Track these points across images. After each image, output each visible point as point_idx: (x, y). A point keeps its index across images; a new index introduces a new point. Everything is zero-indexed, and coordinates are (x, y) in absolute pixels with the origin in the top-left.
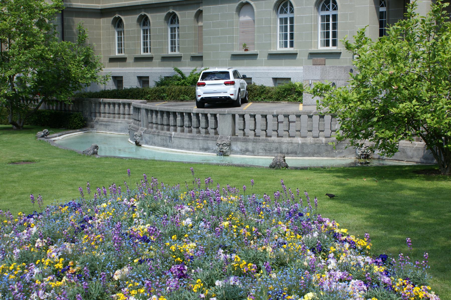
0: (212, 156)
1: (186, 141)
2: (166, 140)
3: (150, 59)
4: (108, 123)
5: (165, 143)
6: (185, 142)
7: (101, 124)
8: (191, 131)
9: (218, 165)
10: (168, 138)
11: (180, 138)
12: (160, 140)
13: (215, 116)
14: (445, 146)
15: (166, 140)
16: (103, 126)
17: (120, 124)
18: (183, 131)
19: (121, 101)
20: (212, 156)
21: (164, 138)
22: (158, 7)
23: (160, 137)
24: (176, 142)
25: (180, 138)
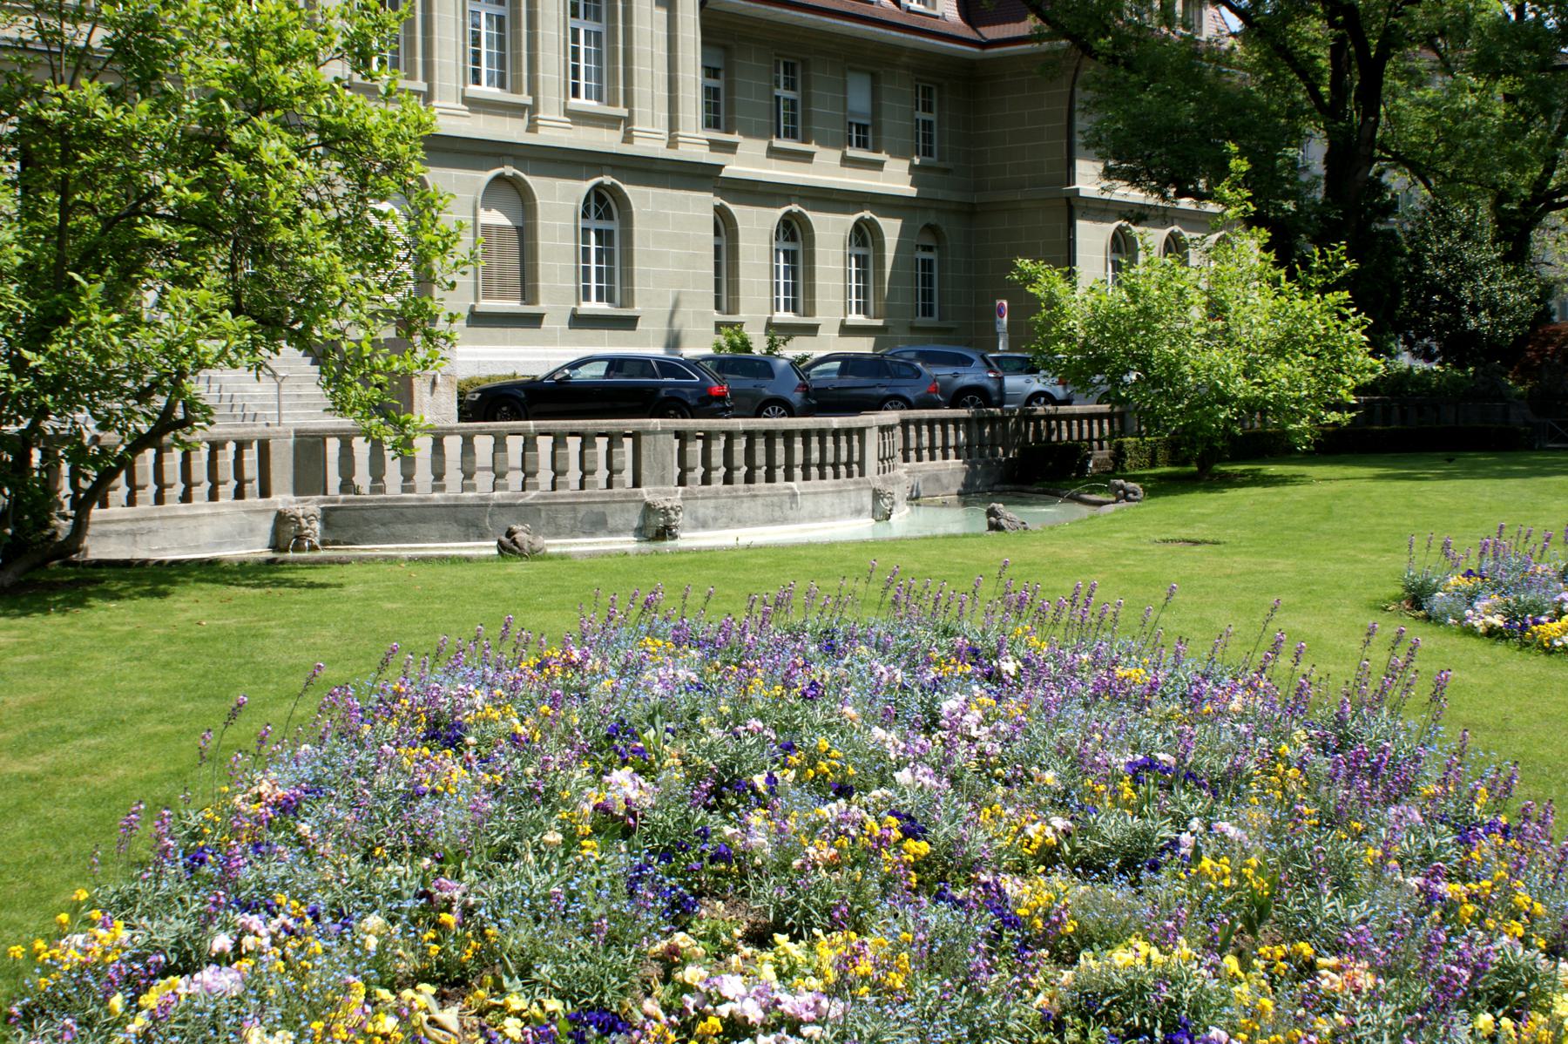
0: (861, 527)
1: (828, 499)
2: (781, 507)
3: (535, 320)
4: (143, 524)
5: (777, 514)
6: (826, 502)
7: (104, 535)
8: (837, 476)
9: (965, 536)
10: (786, 499)
11: (816, 493)
12: (760, 509)
13: (636, 436)
14: (60, 453)
15: (781, 507)
16: (113, 540)
17: (208, 520)
18: (822, 476)
19: (836, 422)
20: (861, 527)
21: (775, 499)
22: (761, 193)
23: (760, 501)
24: (807, 504)
25: (816, 493)
